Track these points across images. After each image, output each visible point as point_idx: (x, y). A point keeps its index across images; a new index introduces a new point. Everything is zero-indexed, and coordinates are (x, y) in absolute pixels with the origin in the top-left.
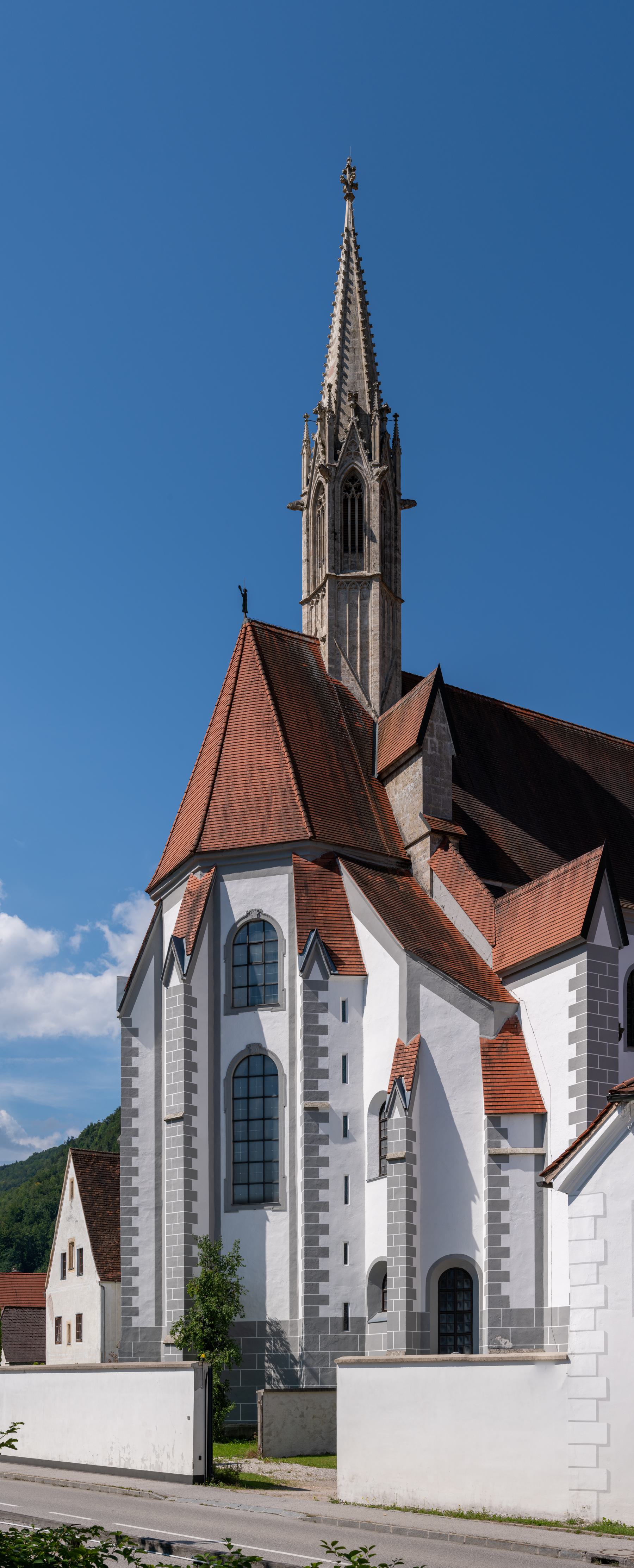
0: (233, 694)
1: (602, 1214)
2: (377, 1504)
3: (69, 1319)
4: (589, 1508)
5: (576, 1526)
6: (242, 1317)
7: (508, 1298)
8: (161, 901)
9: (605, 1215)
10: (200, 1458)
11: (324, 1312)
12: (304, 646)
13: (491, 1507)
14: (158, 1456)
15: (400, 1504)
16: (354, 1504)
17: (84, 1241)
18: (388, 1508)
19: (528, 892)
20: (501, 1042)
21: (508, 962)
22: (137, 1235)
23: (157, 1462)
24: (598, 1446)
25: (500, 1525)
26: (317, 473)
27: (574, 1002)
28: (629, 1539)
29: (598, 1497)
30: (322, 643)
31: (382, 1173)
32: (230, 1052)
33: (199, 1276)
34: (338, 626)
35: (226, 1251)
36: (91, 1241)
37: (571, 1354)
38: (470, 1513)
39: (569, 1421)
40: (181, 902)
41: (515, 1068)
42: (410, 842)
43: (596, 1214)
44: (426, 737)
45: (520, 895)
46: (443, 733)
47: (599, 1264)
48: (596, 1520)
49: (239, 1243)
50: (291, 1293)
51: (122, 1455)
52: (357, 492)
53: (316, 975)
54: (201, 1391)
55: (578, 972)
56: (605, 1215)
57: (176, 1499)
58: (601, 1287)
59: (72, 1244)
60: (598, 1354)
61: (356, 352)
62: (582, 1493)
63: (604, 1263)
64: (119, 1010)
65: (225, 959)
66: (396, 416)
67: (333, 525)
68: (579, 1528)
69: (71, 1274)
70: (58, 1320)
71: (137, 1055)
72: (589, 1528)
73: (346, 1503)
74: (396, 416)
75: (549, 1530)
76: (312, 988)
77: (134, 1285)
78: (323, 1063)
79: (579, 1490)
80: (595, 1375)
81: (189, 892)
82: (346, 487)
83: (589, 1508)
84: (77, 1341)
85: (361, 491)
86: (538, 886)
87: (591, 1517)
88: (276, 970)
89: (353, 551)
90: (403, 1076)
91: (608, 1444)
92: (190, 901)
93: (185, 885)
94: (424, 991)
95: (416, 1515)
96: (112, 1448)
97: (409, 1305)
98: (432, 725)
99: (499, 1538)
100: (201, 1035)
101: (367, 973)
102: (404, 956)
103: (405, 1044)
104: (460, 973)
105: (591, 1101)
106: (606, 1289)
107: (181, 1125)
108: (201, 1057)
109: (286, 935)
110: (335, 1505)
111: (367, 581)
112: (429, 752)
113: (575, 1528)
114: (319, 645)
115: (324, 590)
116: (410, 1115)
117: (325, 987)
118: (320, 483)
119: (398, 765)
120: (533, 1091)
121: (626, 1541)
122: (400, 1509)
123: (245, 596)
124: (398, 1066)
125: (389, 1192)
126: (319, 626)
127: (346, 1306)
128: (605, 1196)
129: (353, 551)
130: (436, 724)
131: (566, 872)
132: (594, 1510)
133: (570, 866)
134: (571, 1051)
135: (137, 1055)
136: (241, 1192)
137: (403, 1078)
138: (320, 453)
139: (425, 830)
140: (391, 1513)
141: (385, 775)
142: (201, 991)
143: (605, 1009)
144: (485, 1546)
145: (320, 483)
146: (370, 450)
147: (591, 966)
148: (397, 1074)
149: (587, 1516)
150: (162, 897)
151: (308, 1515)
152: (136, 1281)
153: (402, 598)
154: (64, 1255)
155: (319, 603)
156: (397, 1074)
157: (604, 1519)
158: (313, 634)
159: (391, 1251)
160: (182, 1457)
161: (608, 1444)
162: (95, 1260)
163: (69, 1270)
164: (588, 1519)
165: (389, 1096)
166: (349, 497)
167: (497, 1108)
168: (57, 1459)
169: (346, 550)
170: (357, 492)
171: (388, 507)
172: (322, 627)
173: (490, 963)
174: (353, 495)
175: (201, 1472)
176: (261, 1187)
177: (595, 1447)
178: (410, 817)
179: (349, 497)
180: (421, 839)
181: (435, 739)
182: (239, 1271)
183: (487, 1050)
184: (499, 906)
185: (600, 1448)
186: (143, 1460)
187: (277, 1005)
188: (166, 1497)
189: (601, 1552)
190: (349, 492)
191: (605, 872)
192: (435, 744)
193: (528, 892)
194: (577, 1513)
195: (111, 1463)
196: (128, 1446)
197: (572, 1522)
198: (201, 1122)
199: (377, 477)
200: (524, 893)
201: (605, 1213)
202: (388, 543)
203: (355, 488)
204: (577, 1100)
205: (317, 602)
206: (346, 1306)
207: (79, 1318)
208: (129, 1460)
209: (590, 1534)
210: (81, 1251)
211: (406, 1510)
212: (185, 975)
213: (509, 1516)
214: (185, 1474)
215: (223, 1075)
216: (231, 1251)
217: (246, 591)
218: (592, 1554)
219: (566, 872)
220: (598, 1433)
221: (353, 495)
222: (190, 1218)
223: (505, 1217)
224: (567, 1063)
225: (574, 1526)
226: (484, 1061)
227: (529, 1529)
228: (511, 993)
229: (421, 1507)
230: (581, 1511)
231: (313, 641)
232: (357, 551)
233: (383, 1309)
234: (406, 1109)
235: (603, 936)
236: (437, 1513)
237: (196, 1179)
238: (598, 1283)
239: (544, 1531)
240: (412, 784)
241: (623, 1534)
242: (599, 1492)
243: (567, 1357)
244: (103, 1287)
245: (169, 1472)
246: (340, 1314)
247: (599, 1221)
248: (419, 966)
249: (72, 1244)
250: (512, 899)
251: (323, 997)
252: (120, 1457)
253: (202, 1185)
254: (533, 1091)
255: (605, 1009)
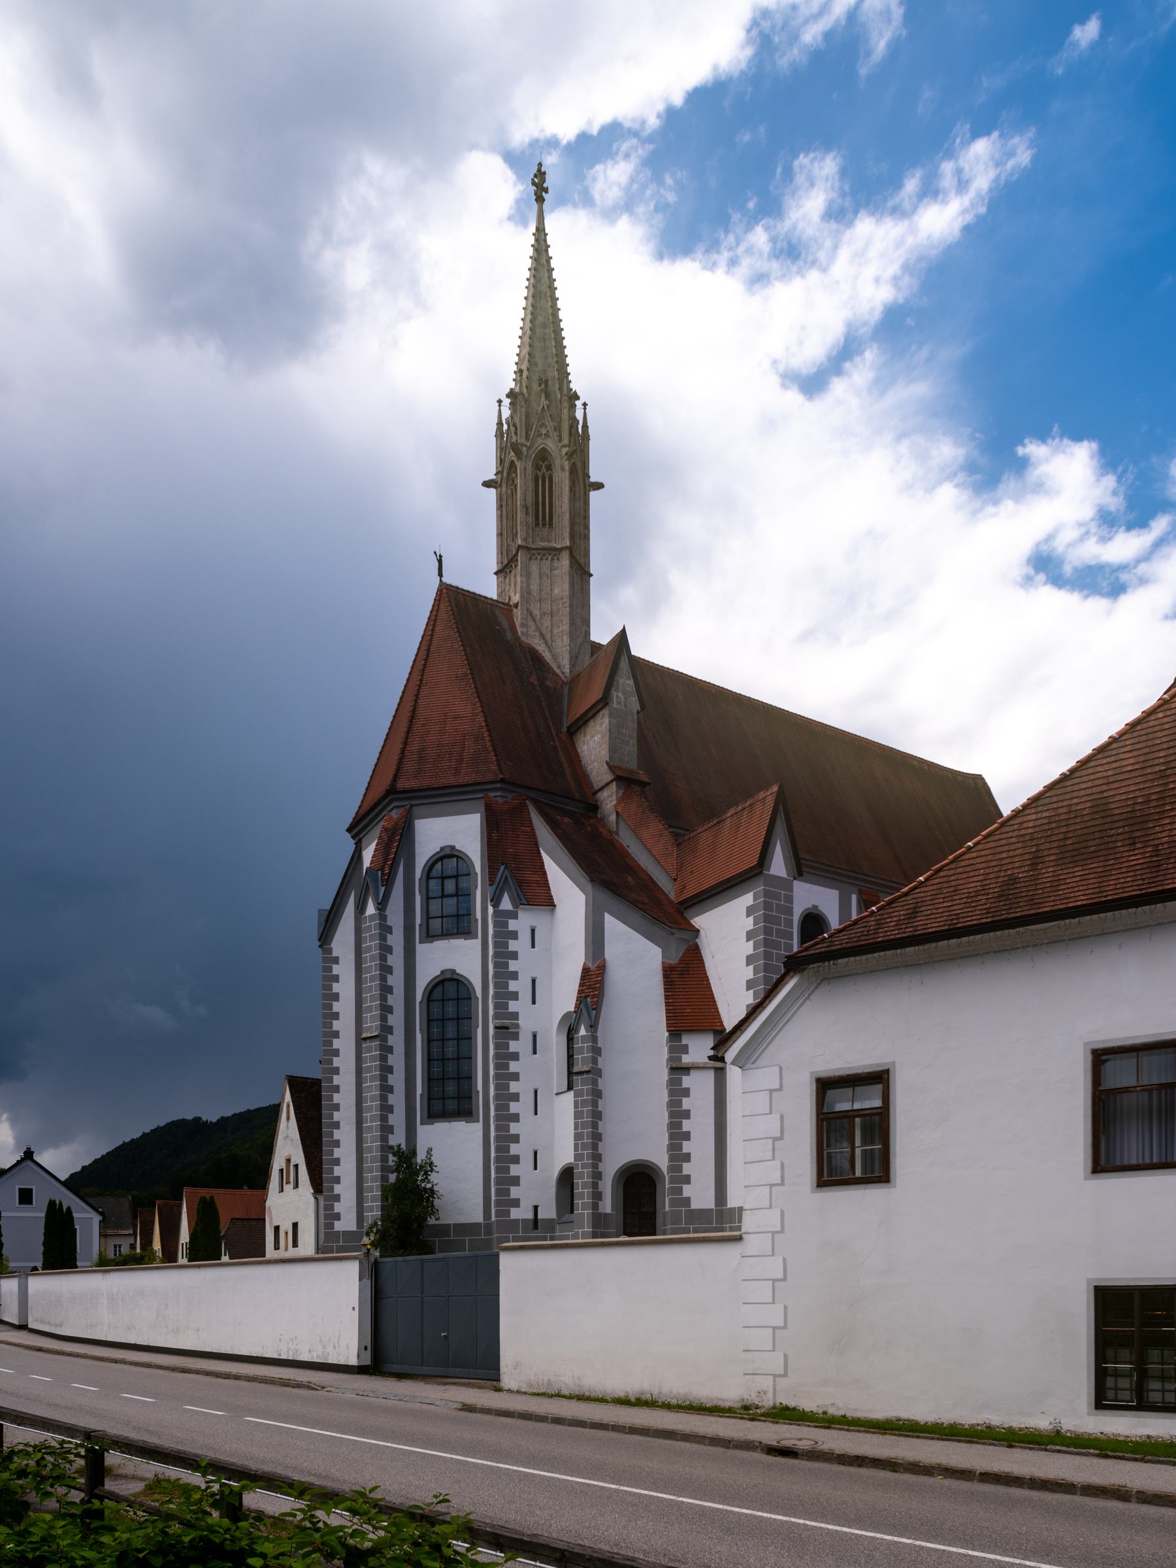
0: (428, 650)
1: (778, 1087)
2: (541, 1391)
3: (286, 1227)
4: (765, 1393)
5: (751, 1412)
6: (436, 1220)
7: (689, 1199)
8: (360, 840)
9: (781, 1089)
10: (366, 1348)
11: (515, 1214)
12: (497, 612)
13: (660, 1393)
14: (324, 1347)
15: (565, 1392)
16: (518, 1392)
17: (299, 1158)
18: (552, 1396)
19: (707, 829)
20: (683, 965)
21: (689, 893)
22: (339, 1147)
23: (323, 1352)
24: (774, 1328)
25: (669, 1413)
26: (509, 453)
27: (752, 927)
28: (809, 1426)
29: (774, 1381)
30: (515, 610)
31: (570, 1088)
32: (425, 976)
33: (393, 1182)
34: (530, 594)
35: (421, 1157)
36: (305, 1157)
37: (745, 1233)
38: (638, 1399)
39: (744, 1303)
40: (376, 841)
41: (696, 990)
42: (597, 788)
43: (771, 1088)
44: (612, 692)
45: (701, 833)
46: (628, 689)
47: (775, 1139)
48: (772, 1405)
49: (431, 1150)
50: (485, 1198)
51: (290, 1346)
52: (547, 471)
53: (506, 904)
54: (368, 1282)
55: (755, 899)
56: (781, 1089)
57: (333, 1389)
58: (777, 1163)
59: (288, 1161)
60: (773, 1233)
61: (547, 342)
62: (757, 1378)
63: (781, 1138)
64: (319, 940)
65: (420, 892)
66: (585, 405)
67: (525, 500)
68: (753, 1414)
69: (288, 1188)
70: (277, 1229)
71: (338, 981)
72: (763, 1415)
73: (509, 1391)
74: (585, 405)
75: (721, 1417)
76: (502, 918)
77: (336, 1192)
78: (513, 986)
79: (754, 1374)
80: (771, 1254)
81: (385, 829)
82: (537, 466)
83: (765, 1393)
84: (293, 1247)
85: (551, 470)
86: (717, 823)
87: (768, 1402)
88: (469, 902)
89: (544, 525)
90: (588, 996)
91: (785, 1327)
92: (385, 837)
93: (382, 823)
94: (610, 921)
95: (580, 1402)
96: (280, 1340)
97: (595, 1206)
98: (618, 681)
99: (665, 1427)
100: (396, 960)
101: (556, 903)
102: (589, 887)
103: (591, 966)
104: (644, 903)
105: (767, 968)
106: (782, 1165)
107: (377, 1043)
108: (396, 980)
109: (478, 869)
110: (497, 1394)
111: (555, 552)
112: (615, 705)
113: (749, 1414)
114: (512, 611)
115: (517, 560)
116: (596, 1031)
117: (516, 917)
118: (512, 463)
119: (586, 718)
120: (713, 1010)
121: (805, 1428)
122: (564, 1397)
123: (440, 561)
124: (584, 988)
125: (576, 1103)
126: (512, 594)
127: (536, 1208)
128: (781, 1068)
129: (544, 525)
130: (621, 681)
131: (743, 809)
132: (770, 1395)
133: (748, 804)
134: (749, 948)
135: (338, 981)
136: (437, 1106)
137: (588, 999)
138: (513, 434)
139: (610, 777)
140: (555, 1401)
141: (574, 729)
142: (395, 916)
143: (781, 934)
144: (649, 1436)
145: (512, 463)
146: (560, 432)
147: (766, 894)
148: (583, 995)
149: (763, 1401)
150: (361, 836)
151: (464, 1405)
152: (338, 1189)
153: (592, 572)
154: (281, 1171)
155: (513, 573)
156: (583, 995)
157: (781, 1403)
158: (507, 601)
159: (577, 1157)
160: (348, 1348)
161: (785, 1327)
162: (309, 1174)
163: (287, 1183)
164: (764, 1404)
165: (575, 1015)
166: (540, 474)
167: (679, 1025)
168: (230, 1352)
169: (537, 524)
170: (547, 471)
171: (578, 488)
172: (515, 595)
173: (672, 896)
174: (543, 474)
175: (367, 1361)
176: (456, 1101)
177: (771, 1329)
178: (598, 766)
179: (540, 474)
180: (607, 784)
181: (620, 694)
182: (433, 1177)
183: (669, 973)
184: (680, 844)
185: (776, 1235)
186: (310, 1351)
187: (469, 933)
188: (323, 1388)
189: (778, 1442)
190: (540, 471)
191: (781, 808)
192: (621, 699)
193: (707, 829)
194: (753, 1398)
195: (280, 1355)
196: (296, 1338)
197: (746, 1408)
198: (397, 1040)
199: (566, 457)
200: (704, 831)
201: (781, 1086)
202: (578, 520)
203: (546, 467)
204: (754, 992)
205: (510, 572)
206: (536, 1208)
207: (295, 1225)
208: (297, 1351)
209: (765, 1421)
210: (296, 1166)
211: (570, 1397)
212: (379, 904)
213: (680, 1402)
214: (350, 1364)
215: (419, 998)
216: (424, 1158)
217: (441, 556)
218: (768, 1445)
219: (743, 809)
220: (775, 1316)
221: (543, 474)
222: (386, 1129)
223: (686, 1125)
224: (745, 983)
225: (747, 1411)
226: (666, 983)
227: (699, 1416)
228: (692, 922)
229: (587, 1394)
230: (757, 1396)
231: (506, 607)
232: (547, 525)
233: (572, 1212)
234: (591, 1026)
235: (778, 866)
236: (602, 1400)
237: (392, 1093)
238: (774, 1159)
239: (716, 1418)
240: (599, 736)
241: (802, 1420)
242: (775, 1376)
243: (741, 1236)
244: (316, 1198)
245: (335, 1362)
246: (531, 1216)
247: (774, 1094)
248: (604, 896)
249: (288, 1161)
250: (693, 837)
251: (513, 925)
252: (288, 1349)
253: (397, 1099)
254: (713, 1010)
255: (781, 934)
